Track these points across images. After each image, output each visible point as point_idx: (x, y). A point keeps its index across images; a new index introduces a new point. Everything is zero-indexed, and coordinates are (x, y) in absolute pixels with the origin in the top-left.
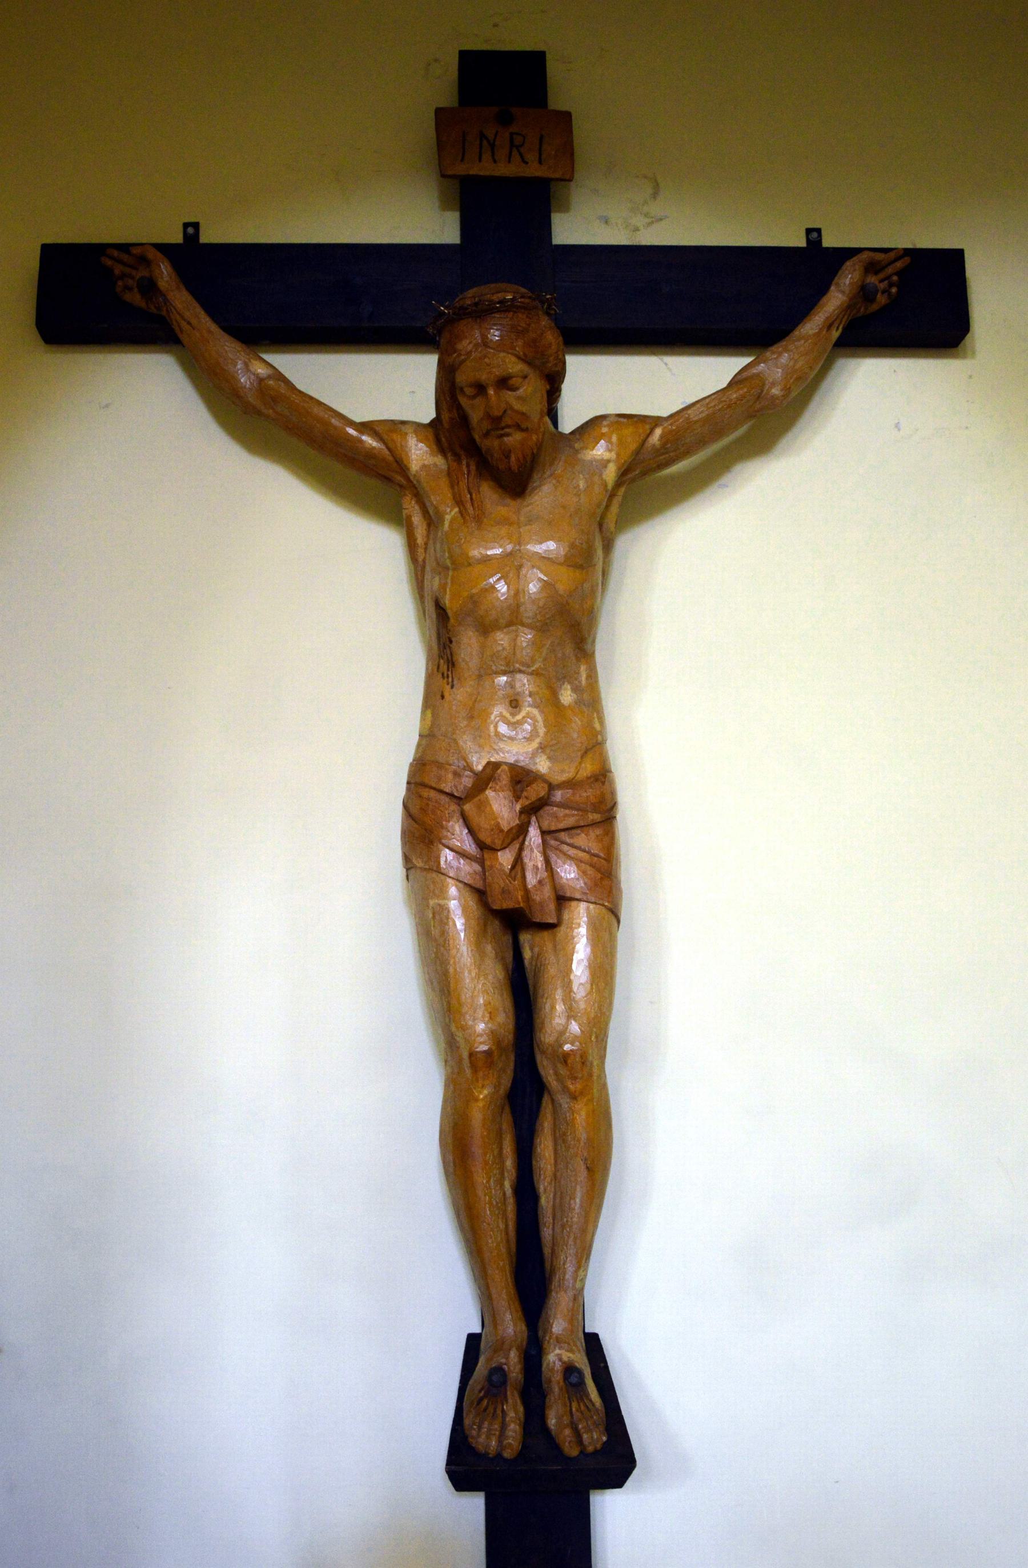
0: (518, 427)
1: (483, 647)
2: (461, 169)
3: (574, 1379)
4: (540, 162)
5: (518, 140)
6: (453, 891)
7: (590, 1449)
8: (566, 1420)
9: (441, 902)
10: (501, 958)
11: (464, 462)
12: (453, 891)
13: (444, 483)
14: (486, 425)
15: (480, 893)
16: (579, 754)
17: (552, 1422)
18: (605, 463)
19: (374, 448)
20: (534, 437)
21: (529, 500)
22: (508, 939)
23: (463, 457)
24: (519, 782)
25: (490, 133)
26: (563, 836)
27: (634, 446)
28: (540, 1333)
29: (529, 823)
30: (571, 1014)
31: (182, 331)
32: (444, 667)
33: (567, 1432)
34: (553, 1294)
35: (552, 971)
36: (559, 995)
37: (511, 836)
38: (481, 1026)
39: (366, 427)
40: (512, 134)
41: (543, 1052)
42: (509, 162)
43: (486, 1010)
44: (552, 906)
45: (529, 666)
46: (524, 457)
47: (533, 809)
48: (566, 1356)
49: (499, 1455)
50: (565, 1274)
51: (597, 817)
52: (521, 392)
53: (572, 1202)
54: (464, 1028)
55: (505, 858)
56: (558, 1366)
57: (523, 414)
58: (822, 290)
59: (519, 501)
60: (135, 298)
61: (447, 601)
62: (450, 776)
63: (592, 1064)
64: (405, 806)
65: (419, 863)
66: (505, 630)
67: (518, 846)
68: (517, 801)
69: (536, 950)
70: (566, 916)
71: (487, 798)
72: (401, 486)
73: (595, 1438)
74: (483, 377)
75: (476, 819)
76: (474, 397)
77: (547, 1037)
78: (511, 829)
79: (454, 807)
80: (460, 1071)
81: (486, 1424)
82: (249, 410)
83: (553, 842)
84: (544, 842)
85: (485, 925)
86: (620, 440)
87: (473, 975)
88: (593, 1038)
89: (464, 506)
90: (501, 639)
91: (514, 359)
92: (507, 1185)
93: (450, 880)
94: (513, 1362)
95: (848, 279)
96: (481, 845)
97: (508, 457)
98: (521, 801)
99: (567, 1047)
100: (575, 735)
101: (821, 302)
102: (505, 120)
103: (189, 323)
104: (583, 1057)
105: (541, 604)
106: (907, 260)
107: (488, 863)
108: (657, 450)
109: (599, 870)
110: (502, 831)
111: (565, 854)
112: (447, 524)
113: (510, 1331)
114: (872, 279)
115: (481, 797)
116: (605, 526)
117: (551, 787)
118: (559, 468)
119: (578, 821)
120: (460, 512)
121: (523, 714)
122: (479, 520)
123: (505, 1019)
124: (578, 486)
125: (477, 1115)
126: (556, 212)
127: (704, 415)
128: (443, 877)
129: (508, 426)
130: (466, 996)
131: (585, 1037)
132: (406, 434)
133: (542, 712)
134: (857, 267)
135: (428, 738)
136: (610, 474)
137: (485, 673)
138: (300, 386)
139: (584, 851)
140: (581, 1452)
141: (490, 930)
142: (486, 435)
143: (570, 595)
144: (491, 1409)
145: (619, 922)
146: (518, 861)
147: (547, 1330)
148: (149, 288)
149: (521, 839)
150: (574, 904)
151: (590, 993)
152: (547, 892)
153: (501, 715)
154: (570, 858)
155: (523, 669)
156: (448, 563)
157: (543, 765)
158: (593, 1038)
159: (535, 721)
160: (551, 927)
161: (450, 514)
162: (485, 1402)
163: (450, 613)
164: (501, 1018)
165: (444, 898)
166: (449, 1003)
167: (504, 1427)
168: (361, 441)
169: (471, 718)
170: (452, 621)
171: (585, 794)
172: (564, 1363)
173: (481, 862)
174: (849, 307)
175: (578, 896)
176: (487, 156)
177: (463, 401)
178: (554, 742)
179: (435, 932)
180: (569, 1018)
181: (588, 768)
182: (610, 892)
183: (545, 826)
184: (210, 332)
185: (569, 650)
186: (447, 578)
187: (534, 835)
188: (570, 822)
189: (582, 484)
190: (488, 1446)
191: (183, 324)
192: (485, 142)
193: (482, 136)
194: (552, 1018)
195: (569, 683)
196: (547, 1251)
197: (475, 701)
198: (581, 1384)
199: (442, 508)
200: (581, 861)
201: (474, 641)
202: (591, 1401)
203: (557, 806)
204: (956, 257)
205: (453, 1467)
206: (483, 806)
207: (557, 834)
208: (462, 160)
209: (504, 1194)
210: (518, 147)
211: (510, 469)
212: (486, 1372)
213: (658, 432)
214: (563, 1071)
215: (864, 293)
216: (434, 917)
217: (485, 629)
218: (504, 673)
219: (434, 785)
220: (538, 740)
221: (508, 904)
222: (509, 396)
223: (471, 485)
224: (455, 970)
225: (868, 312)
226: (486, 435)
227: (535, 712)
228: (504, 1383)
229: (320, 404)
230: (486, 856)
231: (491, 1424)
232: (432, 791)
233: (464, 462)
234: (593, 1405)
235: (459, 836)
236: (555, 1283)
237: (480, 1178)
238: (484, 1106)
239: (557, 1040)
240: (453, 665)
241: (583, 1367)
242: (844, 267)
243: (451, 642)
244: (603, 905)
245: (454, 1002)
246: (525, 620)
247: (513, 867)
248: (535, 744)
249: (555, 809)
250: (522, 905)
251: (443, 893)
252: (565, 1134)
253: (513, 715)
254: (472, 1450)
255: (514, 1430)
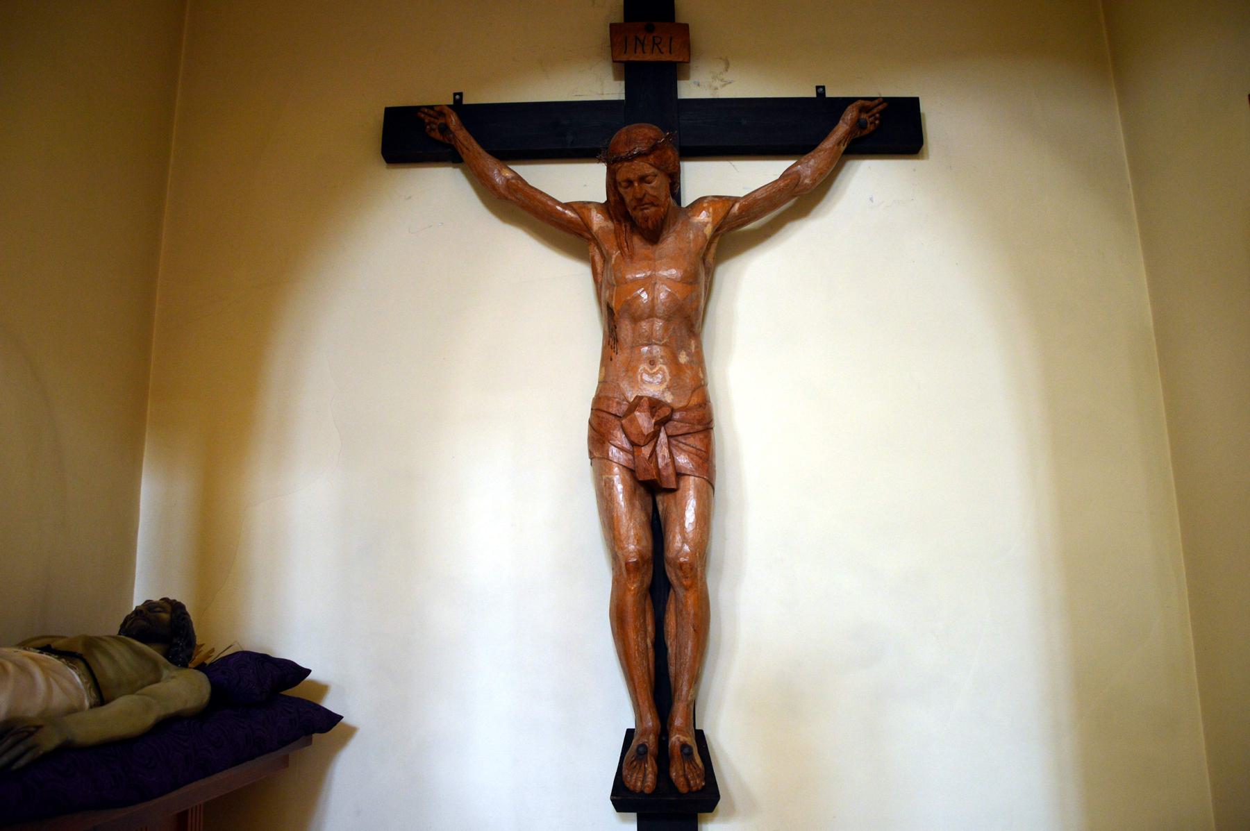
0: (652, 204)
1: (634, 330)
2: (624, 58)
3: (686, 750)
4: (670, 52)
5: (658, 40)
6: (616, 470)
7: (694, 789)
8: (681, 773)
9: (610, 477)
10: (644, 508)
11: (623, 224)
12: (616, 470)
13: (612, 237)
14: (634, 204)
15: (631, 471)
16: (690, 391)
17: (673, 775)
18: (705, 224)
19: (572, 217)
20: (662, 210)
21: (661, 246)
22: (649, 500)
23: (622, 221)
24: (654, 407)
25: (641, 38)
26: (680, 438)
27: (722, 214)
28: (668, 727)
29: (660, 431)
30: (685, 540)
31: (463, 153)
32: (612, 343)
33: (682, 779)
34: (676, 704)
35: (674, 516)
36: (678, 529)
37: (649, 439)
38: (632, 547)
39: (568, 206)
40: (654, 37)
41: (669, 564)
42: (652, 52)
43: (635, 537)
44: (673, 478)
45: (661, 341)
46: (657, 221)
47: (662, 423)
48: (682, 738)
49: (642, 792)
50: (681, 692)
51: (700, 428)
52: (653, 184)
53: (686, 650)
54: (622, 549)
55: (646, 451)
56: (677, 743)
57: (655, 197)
58: (835, 122)
59: (655, 247)
60: (437, 135)
61: (613, 304)
62: (615, 404)
63: (697, 569)
64: (590, 423)
65: (597, 454)
66: (647, 320)
67: (653, 444)
68: (653, 418)
69: (665, 504)
70: (682, 484)
71: (635, 416)
72: (588, 239)
73: (697, 783)
74: (631, 176)
75: (633, 430)
76: (626, 188)
77: (670, 554)
78: (650, 433)
79: (617, 422)
80: (621, 574)
81: (635, 775)
82: (501, 197)
83: (674, 442)
84: (669, 442)
85: (635, 490)
86: (714, 210)
87: (628, 518)
88: (697, 555)
89: (623, 250)
90: (645, 325)
91: (648, 166)
92: (649, 641)
93: (614, 464)
94: (651, 740)
95: (850, 115)
96: (633, 444)
97: (647, 221)
98: (655, 418)
99: (682, 559)
100: (688, 381)
101: (835, 129)
102: (650, 29)
103: (467, 149)
104: (692, 567)
105: (667, 304)
106: (885, 104)
107: (636, 454)
108: (736, 216)
109: (701, 458)
110: (644, 435)
111: (681, 449)
112: (613, 260)
113: (650, 724)
114: (864, 116)
115: (632, 415)
116: (707, 260)
117: (673, 411)
118: (678, 227)
119: (689, 430)
120: (621, 253)
121: (657, 368)
122: (631, 257)
123: (647, 544)
124: (689, 237)
125: (630, 599)
126: (680, 80)
127: (764, 196)
128: (610, 462)
129: (646, 204)
130: (623, 531)
131: (693, 553)
132: (591, 209)
133: (669, 367)
134: (854, 109)
135: (604, 383)
136: (708, 230)
137: (636, 346)
138: (530, 184)
139: (693, 447)
140: (689, 791)
141: (638, 492)
142: (635, 209)
143: (685, 299)
144: (638, 767)
145: (714, 489)
146: (654, 453)
147: (671, 724)
148: (445, 129)
149: (655, 440)
150: (687, 477)
151: (696, 528)
152: (670, 470)
153: (644, 369)
154: (684, 451)
155: (658, 342)
156: (614, 283)
157: (668, 398)
158: (697, 555)
159: (664, 372)
160: (674, 491)
161: (616, 254)
162: (635, 763)
163: (615, 312)
164: (644, 543)
165: (610, 474)
166: (614, 534)
167: (645, 776)
168: (565, 214)
169: (627, 371)
170: (616, 315)
171: (693, 415)
172: (681, 742)
173: (632, 453)
174: (850, 133)
175: (689, 473)
176: (639, 50)
177: (621, 190)
178: (675, 385)
179: (606, 494)
180: (683, 543)
181: (695, 400)
182: (707, 470)
183: (670, 432)
184: (479, 153)
185: (684, 332)
186: (613, 291)
187: (663, 436)
188: (685, 430)
189: (691, 236)
190: (635, 786)
191: (465, 150)
192: (638, 42)
193: (637, 38)
194: (674, 543)
195: (685, 351)
196: (672, 680)
197: (630, 361)
198: (690, 754)
199: (611, 251)
200: (691, 453)
201: (629, 327)
202: (696, 763)
203: (677, 421)
204: (914, 103)
205: (615, 797)
206: (633, 420)
207: (677, 438)
208: (625, 53)
209: (647, 646)
210: (657, 45)
211: (648, 227)
212: (635, 747)
213: (737, 206)
214: (680, 574)
215: (858, 125)
216: (605, 485)
217: (636, 320)
218: (647, 345)
219: (605, 410)
220: (666, 384)
221: (648, 477)
222: (647, 187)
223: (627, 238)
224: (617, 515)
225: (862, 135)
226: (635, 209)
227: (665, 367)
228: (646, 753)
229: (541, 193)
230: (635, 450)
231: (638, 774)
232: (605, 413)
233: (623, 224)
234: (698, 766)
235: (620, 438)
236: (676, 697)
237: (632, 635)
238: (634, 594)
239: (677, 555)
240: (617, 341)
241: (693, 746)
242: (847, 110)
243: (616, 328)
244: (703, 478)
245: (616, 533)
246: (658, 315)
247: (651, 456)
248: (664, 386)
249: (675, 423)
250: (655, 477)
251: (610, 471)
252: (682, 611)
253: (651, 369)
254: (627, 789)
255: (650, 778)
